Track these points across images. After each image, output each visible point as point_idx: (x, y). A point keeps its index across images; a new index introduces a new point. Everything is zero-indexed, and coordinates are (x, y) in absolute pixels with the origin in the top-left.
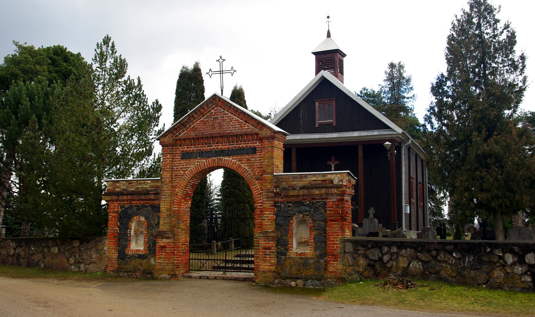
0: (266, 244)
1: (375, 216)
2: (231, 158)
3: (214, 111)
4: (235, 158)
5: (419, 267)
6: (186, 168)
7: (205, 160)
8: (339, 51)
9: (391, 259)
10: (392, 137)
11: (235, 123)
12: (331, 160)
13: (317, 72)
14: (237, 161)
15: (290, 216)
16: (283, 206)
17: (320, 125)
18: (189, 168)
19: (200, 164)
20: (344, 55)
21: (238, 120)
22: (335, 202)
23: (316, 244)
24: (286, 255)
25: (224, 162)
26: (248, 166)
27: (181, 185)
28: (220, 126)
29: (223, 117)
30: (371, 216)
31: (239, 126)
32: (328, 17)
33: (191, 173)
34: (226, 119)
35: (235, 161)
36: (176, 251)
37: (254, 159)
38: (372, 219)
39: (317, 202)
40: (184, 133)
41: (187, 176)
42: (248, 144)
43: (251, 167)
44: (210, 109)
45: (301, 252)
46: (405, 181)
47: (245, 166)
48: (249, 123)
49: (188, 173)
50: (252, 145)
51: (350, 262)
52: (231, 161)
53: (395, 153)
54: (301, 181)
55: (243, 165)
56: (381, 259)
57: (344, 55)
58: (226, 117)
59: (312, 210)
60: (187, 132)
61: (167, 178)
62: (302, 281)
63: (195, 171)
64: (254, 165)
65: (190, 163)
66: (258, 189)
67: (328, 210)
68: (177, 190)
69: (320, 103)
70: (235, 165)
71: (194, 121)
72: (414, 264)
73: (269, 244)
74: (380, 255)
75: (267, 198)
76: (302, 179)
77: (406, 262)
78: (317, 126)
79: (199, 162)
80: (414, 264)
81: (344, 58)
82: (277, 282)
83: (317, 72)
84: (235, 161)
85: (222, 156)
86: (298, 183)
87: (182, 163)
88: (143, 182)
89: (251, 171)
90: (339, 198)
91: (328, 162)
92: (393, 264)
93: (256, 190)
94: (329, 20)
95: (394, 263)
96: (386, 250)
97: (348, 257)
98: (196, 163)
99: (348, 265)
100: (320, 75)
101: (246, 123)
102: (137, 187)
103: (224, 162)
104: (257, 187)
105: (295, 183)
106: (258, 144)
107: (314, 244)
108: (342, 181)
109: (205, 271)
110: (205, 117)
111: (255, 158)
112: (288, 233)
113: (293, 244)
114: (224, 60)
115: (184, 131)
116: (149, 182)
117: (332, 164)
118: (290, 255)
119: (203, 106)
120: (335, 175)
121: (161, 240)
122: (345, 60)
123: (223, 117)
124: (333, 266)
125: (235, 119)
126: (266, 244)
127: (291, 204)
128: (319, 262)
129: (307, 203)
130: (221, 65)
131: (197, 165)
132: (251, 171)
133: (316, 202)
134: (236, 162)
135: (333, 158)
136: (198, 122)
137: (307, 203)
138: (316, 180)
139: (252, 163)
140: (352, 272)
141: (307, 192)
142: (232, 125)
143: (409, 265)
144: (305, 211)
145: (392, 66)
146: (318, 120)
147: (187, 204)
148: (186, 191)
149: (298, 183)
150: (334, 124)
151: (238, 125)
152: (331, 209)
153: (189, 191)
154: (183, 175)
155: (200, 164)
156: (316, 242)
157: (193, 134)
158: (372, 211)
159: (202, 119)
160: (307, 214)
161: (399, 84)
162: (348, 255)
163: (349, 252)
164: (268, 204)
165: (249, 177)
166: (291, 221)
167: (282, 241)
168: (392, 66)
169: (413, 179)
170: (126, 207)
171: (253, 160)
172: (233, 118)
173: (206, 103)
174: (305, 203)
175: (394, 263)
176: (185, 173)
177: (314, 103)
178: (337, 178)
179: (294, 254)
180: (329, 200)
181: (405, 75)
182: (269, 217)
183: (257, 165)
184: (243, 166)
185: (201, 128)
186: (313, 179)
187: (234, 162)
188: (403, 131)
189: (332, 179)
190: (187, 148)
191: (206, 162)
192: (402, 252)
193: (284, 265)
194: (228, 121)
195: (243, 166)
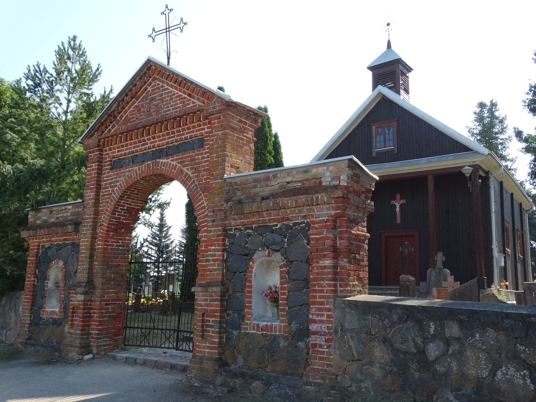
0: (208, 305)
1: (446, 265)
2: (171, 159)
3: (151, 88)
4: (175, 158)
5: (521, 382)
6: (114, 182)
7: (137, 168)
8: (401, 61)
9: (445, 354)
10: (474, 162)
11: (177, 101)
12: (395, 199)
13: (374, 87)
14: (178, 163)
15: (248, 252)
16: (238, 234)
17: (378, 153)
18: (118, 181)
19: (131, 174)
20: (409, 69)
21: (181, 95)
22: (326, 222)
23: (292, 309)
24: (240, 329)
25: (161, 167)
26: (192, 169)
27: (107, 210)
28: (158, 108)
29: (162, 95)
30: (440, 264)
31: (181, 105)
32: (388, 25)
33: (120, 190)
34: (165, 98)
35: (174, 163)
36: (95, 315)
37: (200, 157)
38: (440, 269)
39: (295, 224)
40: (114, 129)
41: (115, 194)
42: (193, 132)
43: (196, 170)
44: (146, 85)
45: (265, 323)
46: (497, 223)
47: (188, 169)
48: (194, 98)
49: (116, 190)
50: (199, 133)
51: (354, 352)
52: (170, 163)
53: (480, 183)
54: (267, 186)
55: (184, 169)
56: (422, 352)
57: (409, 69)
58: (165, 94)
59: (286, 240)
60: (118, 127)
61: (90, 200)
62: (262, 386)
63: (124, 186)
64: (199, 167)
65: (121, 173)
66: (204, 208)
67: (314, 239)
68: (102, 217)
69: (377, 126)
70: (175, 169)
71: (126, 108)
72: (507, 374)
73: (212, 305)
74: (419, 340)
75: (214, 221)
76: (269, 183)
77: (485, 364)
78: (374, 155)
79: (130, 171)
80: (507, 374)
81: (410, 74)
82: (219, 383)
83: (374, 87)
84: (174, 163)
85: (159, 158)
86: (261, 190)
87: (110, 176)
88: (64, 208)
89: (196, 177)
90: (333, 212)
91: (391, 201)
92: (450, 367)
93: (202, 209)
94: (390, 27)
95: (454, 366)
96: (432, 330)
97: (350, 340)
98: (127, 174)
99: (349, 358)
100: (377, 90)
101: (191, 99)
102: (58, 216)
103: (161, 167)
104: (203, 203)
105: (257, 190)
106: (206, 130)
107: (287, 308)
108: (338, 178)
109: (147, 347)
110: (140, 99)
111: (201, 154)
112: (245, 286)
113: (251, 306)
114: (170, 10)
115: (114, 126)
116: (70, 207)
117: (397, 204)
118: (246, 329)
119: (134, 83)
120: (325, 168)
121: (75, 297)
122: (410, 75)
123: (162, 95)
124: (321, 359)
125: (176, 95)
126: (208, 305)
127: (251, 231)
128: (296, 346)
129: (278, 227)
130: (167, 20)
131: (128, 176)
132: (196, 177)
133: (293, 223)
134: (176, 165)
135: (398, 196)
136: (131, 109)
137: (278, 227)
138: (292, 182)
139: (198, 163)
140: (359, 376)
141: (273, 204)
142: (172, 106)
143: (493, 373)
144: (274, 244)
145: (482, 105)
146: (375, 147)
147: (121, 239)
148: (115, 218)
149: (261, 189)
150: (396, 152)
151: (180, 103)
152: (318, 236)
153: (123, 219)
154: (111, 194)
155: (131, 174)
156: (291, 305)
157: (124, 127)
158: (440, 258)
159: (136, 104)
160: (277, 248)
161: (492, 125)
162: (349, 337)
163: (352, 330)
164: (214, 231)
165: (193, 187)
166: (251, 263)
167: (234, 300)
168: (482, 105)
169: (509, 223)
170: (47, 246)
171: (198, 159)
172: (174, 94)
173: (138, 76)
174: (274, 228)
175: (454, 366)
176: (113, 191)
177: (370, 127)
178: (328, 174)
179: (254, 327)
180: (314, 219)
181: (497, 114)
182: (214, 255)
183: (204, 166)
184: (186, 170)
185: (134, 118)
186: (287, 181)
187: (173, 165)
188: (490, 152)
189: (320, 176)
190: (118, 151)
191: (139, 171)
192: (473, 336)
193: (237, 347)
194: (167, 100)
195: (186, 170)
